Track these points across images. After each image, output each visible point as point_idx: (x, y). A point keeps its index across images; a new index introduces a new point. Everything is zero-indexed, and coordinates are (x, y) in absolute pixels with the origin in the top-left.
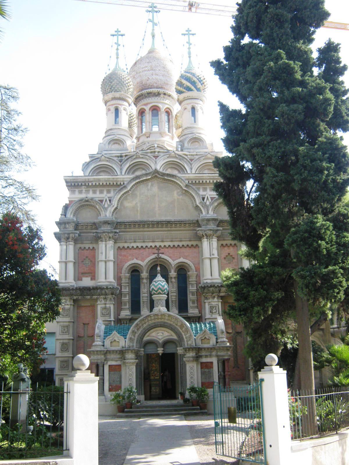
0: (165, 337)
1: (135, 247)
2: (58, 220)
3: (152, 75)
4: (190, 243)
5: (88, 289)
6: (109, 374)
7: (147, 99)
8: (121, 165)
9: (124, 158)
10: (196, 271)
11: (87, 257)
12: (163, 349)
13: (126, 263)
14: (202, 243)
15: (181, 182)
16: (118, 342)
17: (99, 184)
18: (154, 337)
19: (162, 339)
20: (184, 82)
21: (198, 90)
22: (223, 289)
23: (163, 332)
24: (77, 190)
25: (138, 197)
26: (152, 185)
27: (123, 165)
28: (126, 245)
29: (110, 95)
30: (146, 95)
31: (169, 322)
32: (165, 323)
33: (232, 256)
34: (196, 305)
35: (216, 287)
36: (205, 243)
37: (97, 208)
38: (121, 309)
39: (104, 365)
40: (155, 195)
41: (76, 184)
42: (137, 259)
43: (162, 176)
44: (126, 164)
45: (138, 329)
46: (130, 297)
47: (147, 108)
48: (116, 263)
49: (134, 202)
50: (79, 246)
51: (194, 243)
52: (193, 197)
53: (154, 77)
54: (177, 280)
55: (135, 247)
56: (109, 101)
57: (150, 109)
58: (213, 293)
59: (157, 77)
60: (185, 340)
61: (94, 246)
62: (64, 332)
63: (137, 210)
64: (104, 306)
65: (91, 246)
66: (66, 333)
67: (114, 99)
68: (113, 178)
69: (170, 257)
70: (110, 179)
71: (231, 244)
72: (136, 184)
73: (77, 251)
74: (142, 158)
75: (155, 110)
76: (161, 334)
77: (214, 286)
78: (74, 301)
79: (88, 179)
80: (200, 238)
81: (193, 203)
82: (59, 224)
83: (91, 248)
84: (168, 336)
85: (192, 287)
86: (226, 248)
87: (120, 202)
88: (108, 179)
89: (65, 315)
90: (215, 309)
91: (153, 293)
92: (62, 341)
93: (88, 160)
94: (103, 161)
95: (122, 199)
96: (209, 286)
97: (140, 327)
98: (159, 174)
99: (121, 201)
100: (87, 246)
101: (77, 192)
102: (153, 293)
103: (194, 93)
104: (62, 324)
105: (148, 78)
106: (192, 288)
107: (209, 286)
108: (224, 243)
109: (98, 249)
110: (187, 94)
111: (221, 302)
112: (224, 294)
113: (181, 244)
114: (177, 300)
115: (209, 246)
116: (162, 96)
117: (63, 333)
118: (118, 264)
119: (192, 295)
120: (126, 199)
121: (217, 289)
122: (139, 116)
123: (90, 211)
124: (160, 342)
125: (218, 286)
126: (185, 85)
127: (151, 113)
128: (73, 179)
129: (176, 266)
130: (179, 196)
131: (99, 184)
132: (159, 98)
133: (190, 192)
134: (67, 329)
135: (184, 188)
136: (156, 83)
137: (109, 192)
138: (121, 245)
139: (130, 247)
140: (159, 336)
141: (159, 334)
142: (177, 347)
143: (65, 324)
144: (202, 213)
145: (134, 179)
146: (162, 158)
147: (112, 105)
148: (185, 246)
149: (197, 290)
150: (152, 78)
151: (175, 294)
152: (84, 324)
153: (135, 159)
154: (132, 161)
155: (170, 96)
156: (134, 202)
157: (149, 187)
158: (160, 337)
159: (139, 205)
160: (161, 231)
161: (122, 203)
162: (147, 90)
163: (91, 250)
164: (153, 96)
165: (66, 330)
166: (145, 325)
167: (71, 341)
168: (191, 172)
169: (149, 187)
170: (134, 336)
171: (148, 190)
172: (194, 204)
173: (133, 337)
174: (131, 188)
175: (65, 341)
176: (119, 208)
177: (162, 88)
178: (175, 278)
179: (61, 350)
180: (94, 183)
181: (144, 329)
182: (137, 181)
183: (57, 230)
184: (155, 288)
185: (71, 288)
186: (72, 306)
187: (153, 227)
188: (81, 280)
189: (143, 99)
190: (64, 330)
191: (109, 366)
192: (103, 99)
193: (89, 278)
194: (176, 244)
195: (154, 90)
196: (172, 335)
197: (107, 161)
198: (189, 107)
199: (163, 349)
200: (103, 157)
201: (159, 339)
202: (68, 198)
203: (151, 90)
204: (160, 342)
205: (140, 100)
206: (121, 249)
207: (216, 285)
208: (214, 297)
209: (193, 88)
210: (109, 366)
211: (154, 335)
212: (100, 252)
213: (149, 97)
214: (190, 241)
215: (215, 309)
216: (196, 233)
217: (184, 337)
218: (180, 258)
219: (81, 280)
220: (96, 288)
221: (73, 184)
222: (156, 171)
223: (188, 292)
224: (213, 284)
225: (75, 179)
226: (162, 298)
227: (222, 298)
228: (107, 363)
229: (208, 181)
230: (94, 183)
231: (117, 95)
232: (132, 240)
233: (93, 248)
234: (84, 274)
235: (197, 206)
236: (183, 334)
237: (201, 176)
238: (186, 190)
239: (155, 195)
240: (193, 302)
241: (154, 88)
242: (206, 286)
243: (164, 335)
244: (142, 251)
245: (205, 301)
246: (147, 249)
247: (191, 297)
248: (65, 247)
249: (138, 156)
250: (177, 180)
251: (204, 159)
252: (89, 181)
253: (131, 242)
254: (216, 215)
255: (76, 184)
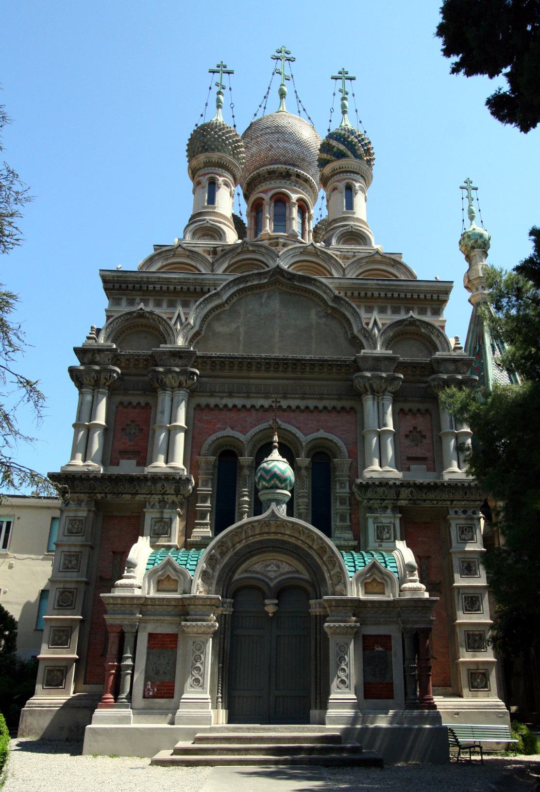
0: (282, 574)
1: (230, 406)
2: (80, 345)
3: (278, 141)
4: (339, 404)
5: (131, 479)
6: (148, 654)
7: (268, 183)
8: (213, 264)
9: (220, 254)
10: (350, 457)
11: (133, 421)
12: (276, 601)
13: (210, 435)
14: (362, 405)
15: (325, 292)
16: (175, 580)
17: (168, 288)
18: (257, 573)
19: (276, 578)
20: (334, 143)
21: (358, 157)
22: (405, 493)
23: (280, 563)
24: (124, 298)
25: (242, 318)
26: (269, 297)
27: (216, 265)
28: (212, 402)
29: (202, 158)
30: (266, 175)
31: (293, 540)
32: (283, 542)
33: (420, 432)
34: (348, 523)
35: (391, 487)
36: (369, 404)
37: (160, 331)
38: (195, 525)
39: (137, 632)
40: (274, 315)
41: (124, 286)
42: (232, 429)
43: (289, 279)
44: (223, 263)
45: (223, 554)
46: (215, 503)
47: (267, 197)
48: (190, 436)
49: (234, 326)
50: (118, 399)
51: (347, 404)
52: (348, 320)
53: (281, 144)
54: (310, 473)
55: (230, 406)
56: (200, 169)
57: (271, 198)
58: (384, 500)
59: (286, 145)
60: (329, 582)
61: (149, 400)
62: (70, 566)
63: (239, 340)
64: (158, 515)
65: (143, 400)
66: (72, 568)
67: (209, 164)
68: (196, 279)
69: (299, 428)
70: (189, 279)
71: (419, 410)
72: (238, 291)
73: (114, 407)
74: (254, 252)
75: (281, 200)
76: (275, 568)
77: (387, 483)
78: (98, 504)
79: (148, 278)
80: (357, 396)
81: (346, 333)
82: (80, 352)
83: (143, 404)
84: (288, 573)
85: (341, 488)
86: (409, 417)
87: (206, 324)
88: (185, 279)
89: (75, 531)
90: (388, 532)
91: (260, 487)
92: (61, 586)
93: (152, 252)
94: (179, 256)
95: (211, 317)
96: (377, 483)
97: (228, 549)
98: (283, 276)
99: (208, 321)
100: (134, 400)
101: (124, 302)
102: (260, 487)
103: (350, 162)
104: (66, 549)
105: (271, 146)
106: (340, 490)
107: (377, 483)
108: (406, 406)
109: (156, 406)
110: (336, 164)
111: (401, 519)
112: (407, 502)
113: (321, 405)
114: (310, 512)
115: (376, 414)
116: (293, 178)
117: (68, 568)
118: (193, 438)
119: (341, 504)
120: (218, 318)
121: (393, 491)
122: (251, 211)
123: (146, 338)
124: (272, 584)
125: (394, 484)
126: (335, 150)
127: (273, 204)
128: (118, 276)
129: (310, 445)
130: (320, 318)
131: (168, 288)
132: (288, 182)
133: (343, 310)
134: (77, 560)
135: (331, 304)
136: (284, 156)
137: (172, 304)
138: (203, 401)
139: (221, 406)
140: (270, 571)
141: (269, 568)
142: (309, 598)
143: (73, 549)
144: (375, 348)
145: (235, 282)
146: (291, 252)
147: (205, 175)
148: (330, 408)
149: (352, 493)
150: (278, 147)
151: (306, 500)
152: (114, 552)
153: (239, 254)
154: (233, 258)
155: (306, 180)
156: (234, 326)
157: (263, 300)
158: (272, 575)
159: (242, 330)
160: (283, 379)
161: (209, 325)
162: (268, 167)
163: (143, 408)
164: (277, 178)
165: (74, 562)
166: (239, 547)
167: (83, 585)
168: (344, 275)
169: (263, 300)
170: (213, 569)
171: (261, 305)
172: (349, 333)
173: (210, 571)
174: (229, 299)
175: (68, 586)
176: (203, 333)
177: (294, 165)
178: (306, 468)
179: (59, 605)
180: (158, 287)
181: (236, 554)
182: (241, 286)
183: (76, 362)
184: (265, 475)
185: (92, 476)
186: (92, 514)
187: (267, 370)
188: (118, 464)
189: (260, 183)
190: (70, 561)
191: (150, 635)
192: (190, 167)
193: (134, 462)
194: (311, 404)
195: (280, 166)
196: (298, 572)
197: (188, 256)
198: (342, 186)
199: (276, 601)
200: (180, 249)
201: (271, 579)
202: (106, 311)
203: (276, 166)
204: (272, 584)
205: (256, 186)
206: (202, 410)
207: (391, 483)
208: (386, 508)
209: (349, 153)
210: (150, 635)
211: (258, 570)
212: (159, 409)
213: (271, 179)
214: (339, 399)
215: (388, 532)
216: (352, 386)
217: (327, 575)
218: (318, 430)
219: (118, 464)
220: (145, 479)
221: (117, 286)
222: (279, 270)
223: (332, 498)
224: (385, 481)
225: (121, 277)
226: (280, 497)
227: (397, 509)
228: (145, 627)
229: (376, 294)
230: (158, 287)
231: (215, 156)
232: (224, 392)
233: (147, 404)
234: (125, 454)
235: (355, 337)
236: (324, 568)
237: (363, 284)
238: (333, 308)
239: (274, 315)
240: (343, 519)
241: (281, 163)
242: (370, 482)
243: (281, 571)
244: (243, 415)
245: (368, 515)
246: (254, 412)
247: (338, 506)
248: (89, 398)
249: (245, 249)
250: (318, 287)
251: (367, 262)
252: (149, 283)
253: (222, 398)
254: (391, 352)
255: (124, 286)
